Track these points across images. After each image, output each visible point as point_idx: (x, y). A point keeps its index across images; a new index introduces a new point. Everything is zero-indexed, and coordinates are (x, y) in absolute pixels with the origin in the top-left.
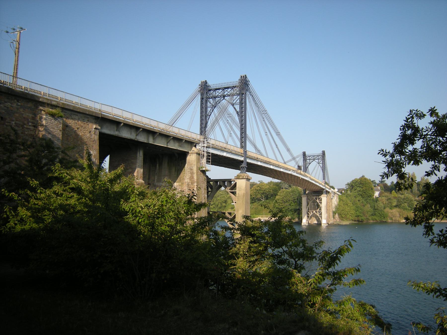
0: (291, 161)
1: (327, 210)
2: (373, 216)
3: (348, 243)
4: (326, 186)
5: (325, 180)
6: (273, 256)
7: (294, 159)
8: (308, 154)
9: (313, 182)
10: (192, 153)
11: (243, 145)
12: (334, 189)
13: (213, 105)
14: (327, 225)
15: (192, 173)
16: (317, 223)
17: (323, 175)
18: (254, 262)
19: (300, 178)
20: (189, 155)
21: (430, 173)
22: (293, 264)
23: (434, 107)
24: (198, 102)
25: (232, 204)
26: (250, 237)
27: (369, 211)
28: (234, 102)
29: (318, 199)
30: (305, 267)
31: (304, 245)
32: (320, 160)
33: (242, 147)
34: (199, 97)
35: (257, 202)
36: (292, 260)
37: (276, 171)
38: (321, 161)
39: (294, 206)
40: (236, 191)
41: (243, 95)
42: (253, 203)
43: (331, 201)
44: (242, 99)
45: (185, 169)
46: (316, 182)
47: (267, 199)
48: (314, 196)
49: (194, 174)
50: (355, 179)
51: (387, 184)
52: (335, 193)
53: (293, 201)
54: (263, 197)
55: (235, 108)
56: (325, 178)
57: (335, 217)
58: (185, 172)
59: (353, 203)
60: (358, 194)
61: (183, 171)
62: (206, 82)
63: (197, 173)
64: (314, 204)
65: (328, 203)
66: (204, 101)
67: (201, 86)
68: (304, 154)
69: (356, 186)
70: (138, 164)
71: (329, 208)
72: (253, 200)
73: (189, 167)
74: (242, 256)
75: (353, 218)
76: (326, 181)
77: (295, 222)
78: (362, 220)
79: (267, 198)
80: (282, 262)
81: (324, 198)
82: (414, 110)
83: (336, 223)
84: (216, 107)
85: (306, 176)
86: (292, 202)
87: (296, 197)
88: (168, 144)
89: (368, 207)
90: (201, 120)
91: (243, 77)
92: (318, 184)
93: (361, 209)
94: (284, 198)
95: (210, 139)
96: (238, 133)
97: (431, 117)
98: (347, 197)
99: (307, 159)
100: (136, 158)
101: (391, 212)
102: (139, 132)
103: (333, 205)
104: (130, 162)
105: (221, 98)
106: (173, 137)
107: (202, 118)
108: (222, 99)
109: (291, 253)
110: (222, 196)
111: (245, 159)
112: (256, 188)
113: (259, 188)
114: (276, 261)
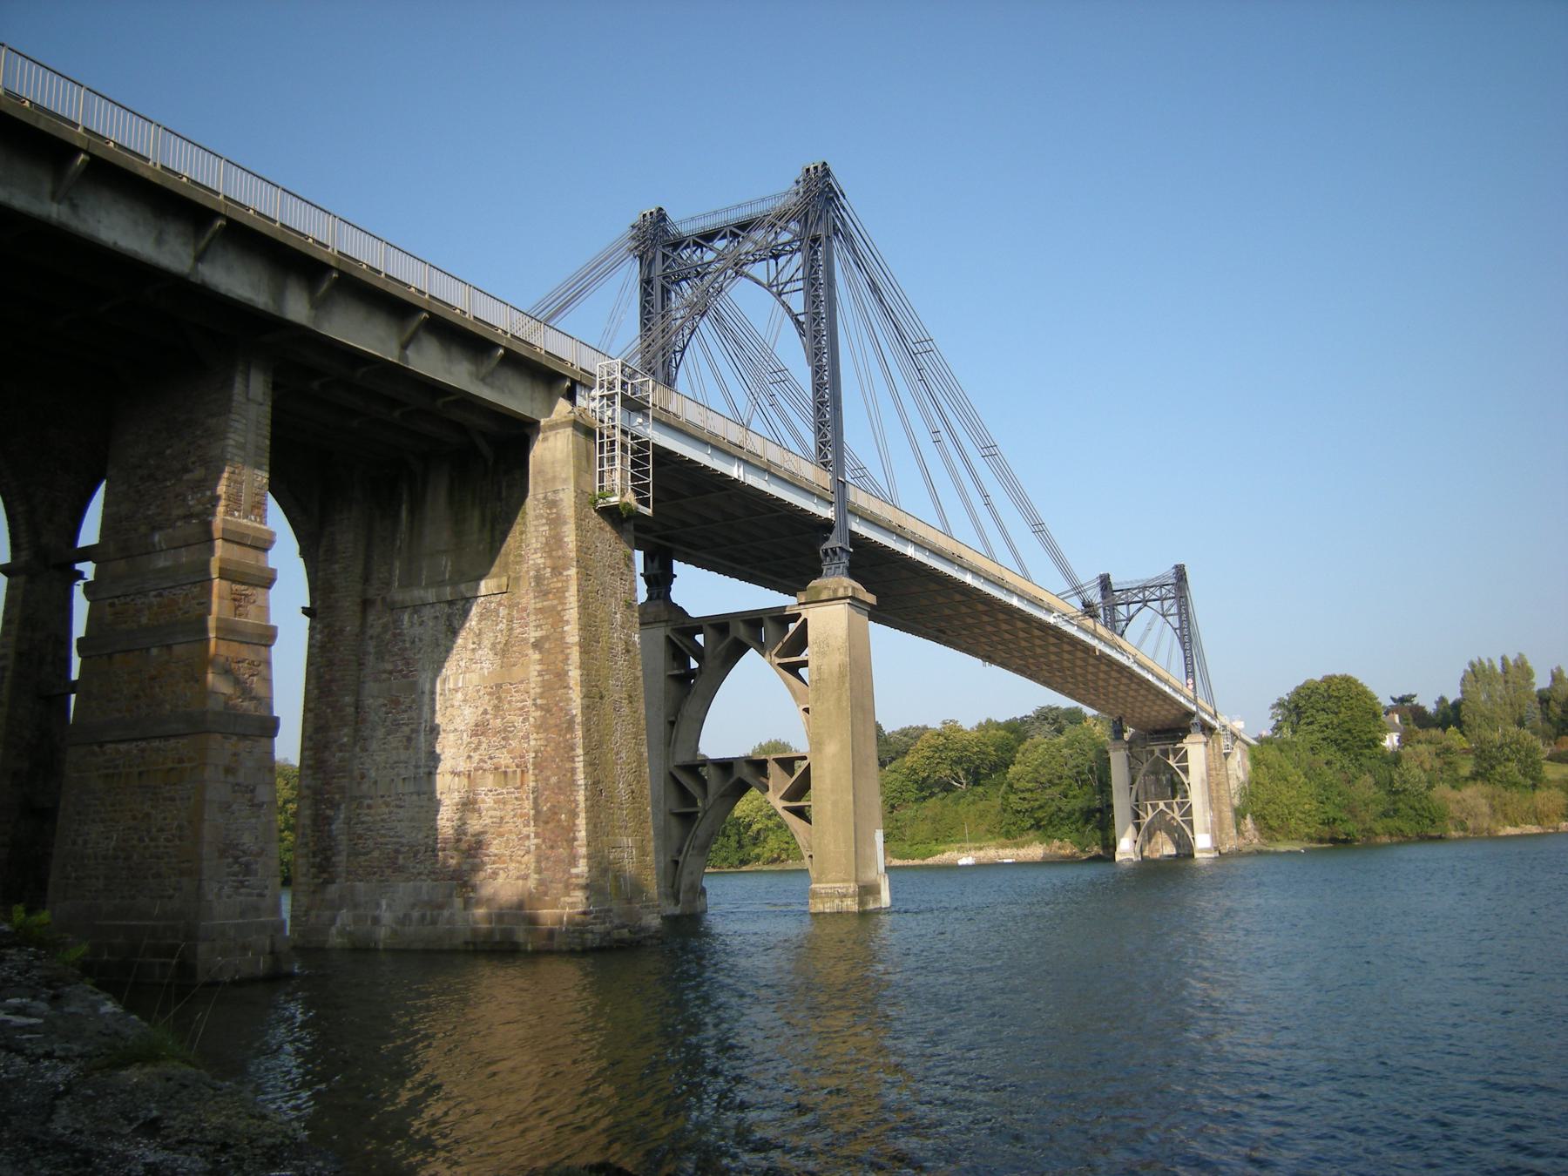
2: (1388, 821)
8: (1122, 584)
9: (1150, 677)
10: (554, 427)
15: (556, 522)
16: (1174, 852)
19: (1093, 649)
20: (541, 436)
27: (1373, 801)
29: (1171, 756)
32: (1167, 604)
35: (940, 795)
39: (1079, 800)
45: (525, 513)
47: (976, 783)
49: (565, 523)
50: (1306, 683)
51: (1423, 708)
53: (1077, 781)
56: (1193, 672)
57: (1242, 827)
59: (1305, 775)
60: (1324, 739)
62: (661, 216)
64: (1158, 780)
65: (1214, 773)
69: (1312, 707)
70: (233, 439)
71: (1218, 791)
73: (540, 496)
75: (1313, 830)
78: (1348, 835)
79: (976, 778)
81: (1195, 749)
83: (1250, 850)
85: (1120, 647)
86: (1070, 785)
87: (1087, 765)
88: (408, 352)
89: (1365, 787)
93: (1339, 795)
98: (1281, 751)
101: (1459, 797)
103: (1234, 784)
104: (198, 433)
106: (430, 313)
112: (932, 741)
113: (941, 738)
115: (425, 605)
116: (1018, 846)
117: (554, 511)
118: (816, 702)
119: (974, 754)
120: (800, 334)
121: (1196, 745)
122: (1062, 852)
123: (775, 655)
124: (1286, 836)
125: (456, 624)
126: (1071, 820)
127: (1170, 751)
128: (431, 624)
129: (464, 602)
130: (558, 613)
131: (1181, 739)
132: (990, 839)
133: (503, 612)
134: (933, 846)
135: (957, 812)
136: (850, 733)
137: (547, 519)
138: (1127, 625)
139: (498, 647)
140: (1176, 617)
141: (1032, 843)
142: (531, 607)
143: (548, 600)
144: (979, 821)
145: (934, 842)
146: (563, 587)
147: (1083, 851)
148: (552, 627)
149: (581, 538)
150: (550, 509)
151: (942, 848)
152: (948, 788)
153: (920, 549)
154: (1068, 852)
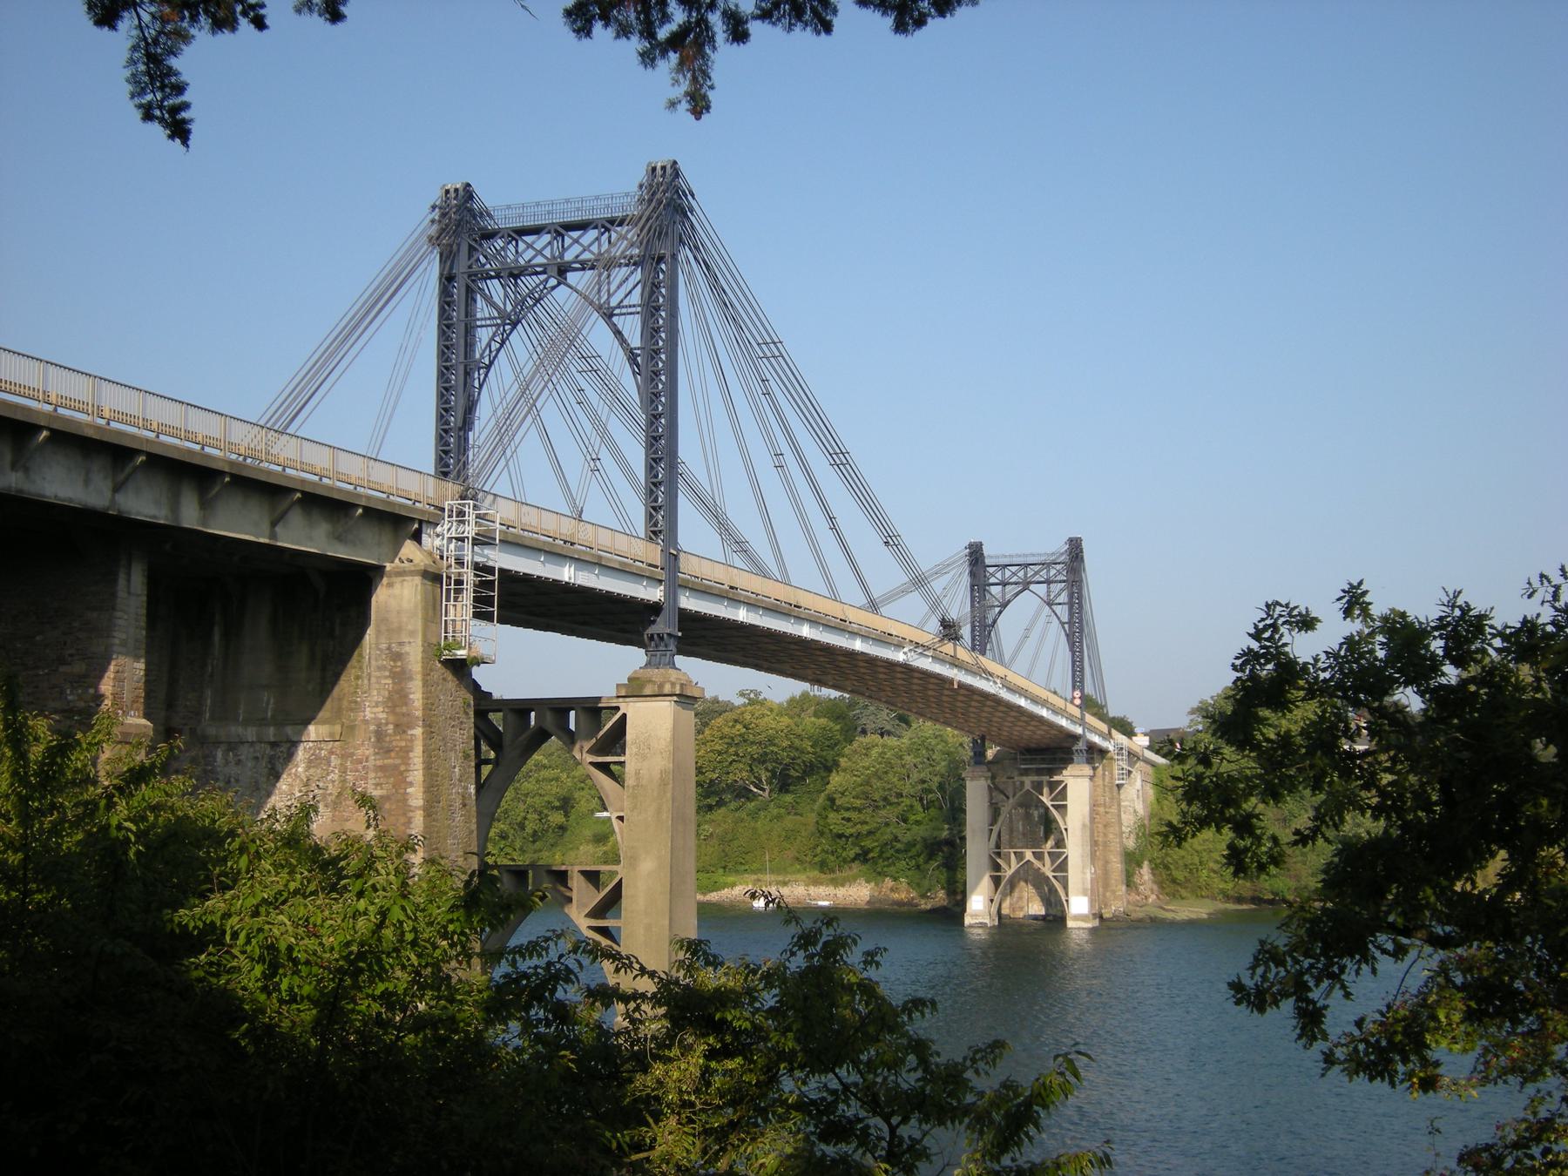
0: (904, 591)
1: (1094, 843)
3: (1065, 1065)
4: (1090, 719)
5: (1082, 691)
6: (801, 1106)
7: (919, 582)
8: (997, 557)
9: (1022, 702)
10: (401, 573)
11: (661, 523)
12: (1129, 731)
13: (503, 315)
14: (1096, 923)
15: (400, 677)
16: (1043, 912)
17: (1074, 662)
18: (722, 1135)
19: (951, 681)
20: (385, 580)
21: (1308, 835)
22: (880, 1139)
23: (1361, 583)
24: (429, 290)
25: (598, 814)
26: (708, 1035)
28: (614, 302)
29: (1046, 790)
30: (934, 1150)
31: (924, 1062)
32: (1056, 588)
33: (653, 534)
34: (432, 271)
35: (733, 805)
36: (876, 1121)
37: (828, 650)
38: (1062, 590)
39: (922, 827)
40: (622, 759)
41: (663, 266)
42: (710, 808)
43: (1112, 798)
44: (655, 286)
45: (361, 655)
46: (1035, 700)
48: (1026, 772)
49: (411, 679)
52: (1133, 756)
53: (921, 799)
54: (764, 779)
55: (618, 333)
56: (1082, 681)
57: (1137, 879)
58: (361, 668)
61: (353, 661)
62: (468, 193)
63: (426, 674)
64: (1028, 816)
65: (1101, 810)
66: (458, 292)
67: (443, 215)
68: (976, 555)
70: (119, 636)
71: (1105, 835)
72: (712, 794)
73: (384, 646)
74: (673, 1112)
76: (1089, 689)
77: (929, 907)
78: (1276, 894)
79: (784, 783)
80: (837, 1131)
81: (1077, 783)
82: (1281, 605)
83: (1141, 915)
84: (519, 321)
85: (985, 671)
87: (937, 779)
88: (278, 529)
90: (444, 391)
91: (659, 172)
92: (1044, 713)
94: (874, 781)
95: (490, 498)
96: (637, 456)
97: (1345, 618)
99: (992, 580)
100: (108, 604)
102: (130, 475)
103: (1128, 820)
104: (76, 624)
105: (546, 281)
106: (303, 492)
107: (448, 380)
108: (553, 282)
109: (875, 1096)
110: (545, 773)
111: (672, 594)
112: (726, 730)
113: (739, 726)
114: (812, 1128)
115: (242, 743)
116: (836, 883)
117: (399, 664)
118: (632, 811)
119: (783, 749)
120: (634, 372)
121: (1079, 780)
122: (896, 896)
123: (588, 752)
124: (1193, 892)
125: (279, 767)
126: (910, 854)
127: (1045, 783)
128: (250, 764)
129: (289, 745)
130: (401, 773)
131: (1059, 771)
132: (799, 871)
133: (335, 761)
134: (719, 876)
135: (755, 830)
136: (669, 850)
137: (391, 671)
138: (1000, 612)
139: (329, 799)
140: (1066, 607)
141: (855, 880)
142: (371, 764)
143: (390, 758)
144: (785, 843)
145: (721, 871)
146: (406, 746)
147: (923, 896)
148: (394, 787)
149: (427, 695)
150: (394, 661)
151: (731, 879)
152: (743, 793)
153: (752, 608)
154: (902, 896)
